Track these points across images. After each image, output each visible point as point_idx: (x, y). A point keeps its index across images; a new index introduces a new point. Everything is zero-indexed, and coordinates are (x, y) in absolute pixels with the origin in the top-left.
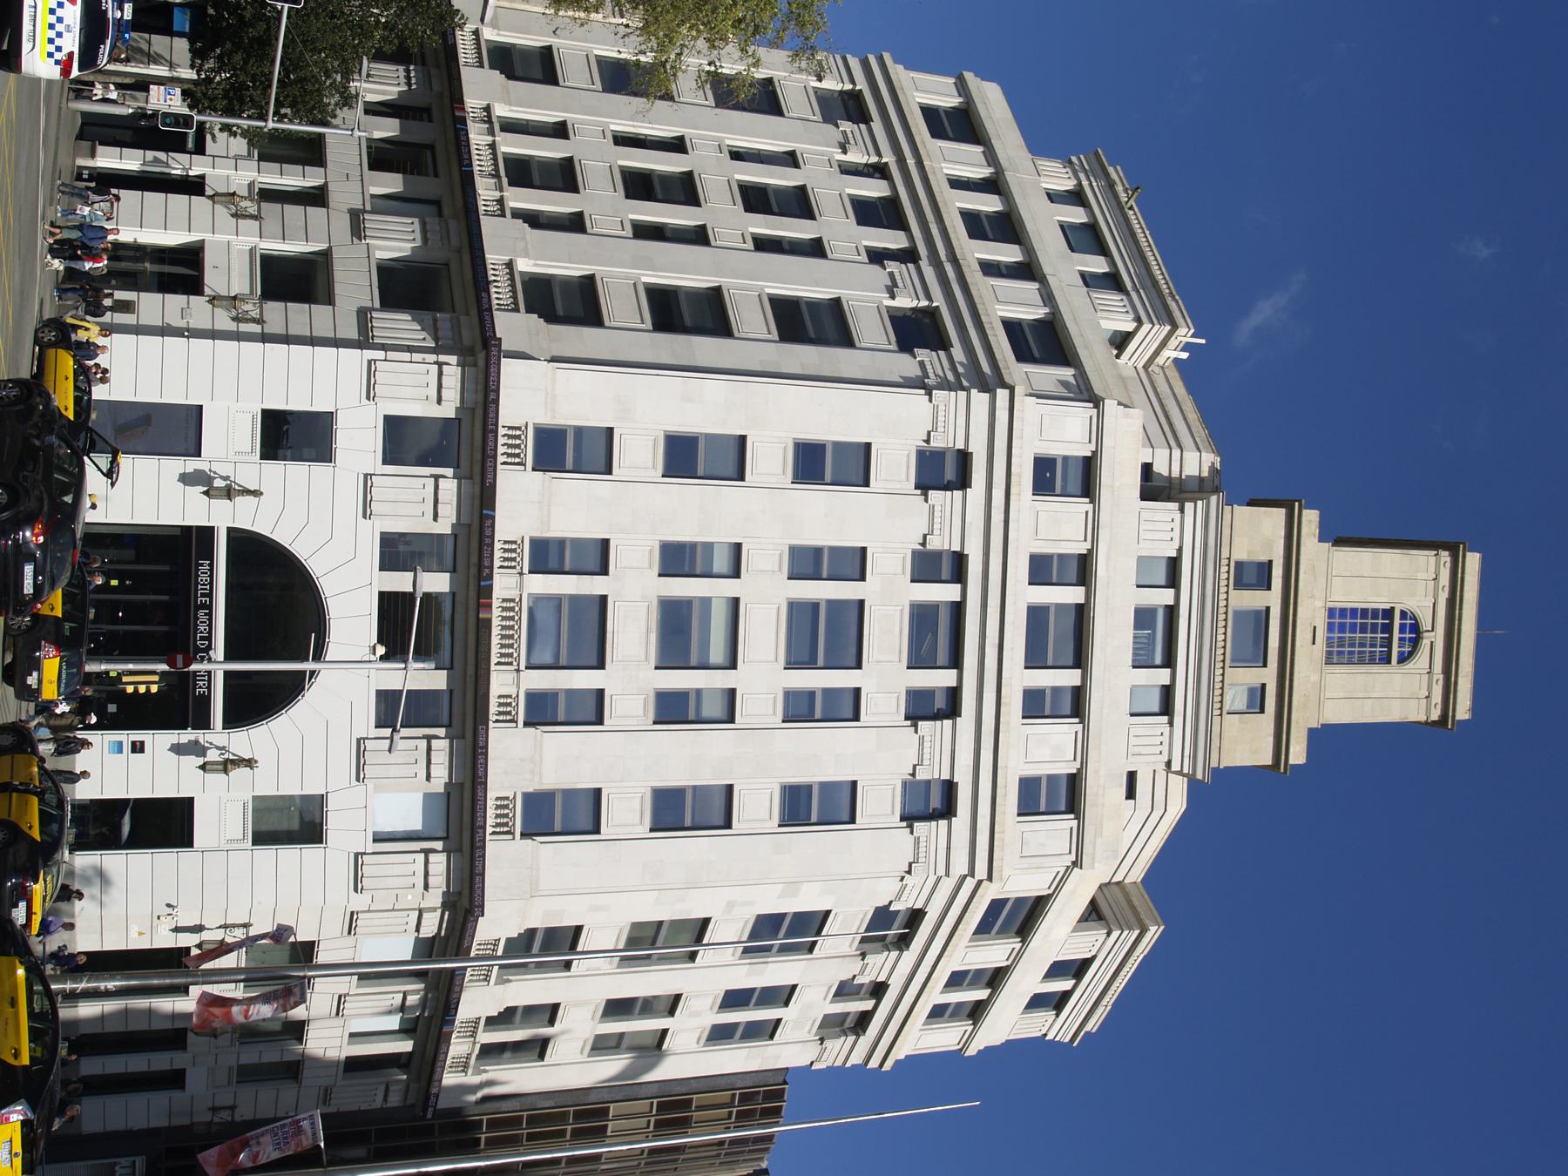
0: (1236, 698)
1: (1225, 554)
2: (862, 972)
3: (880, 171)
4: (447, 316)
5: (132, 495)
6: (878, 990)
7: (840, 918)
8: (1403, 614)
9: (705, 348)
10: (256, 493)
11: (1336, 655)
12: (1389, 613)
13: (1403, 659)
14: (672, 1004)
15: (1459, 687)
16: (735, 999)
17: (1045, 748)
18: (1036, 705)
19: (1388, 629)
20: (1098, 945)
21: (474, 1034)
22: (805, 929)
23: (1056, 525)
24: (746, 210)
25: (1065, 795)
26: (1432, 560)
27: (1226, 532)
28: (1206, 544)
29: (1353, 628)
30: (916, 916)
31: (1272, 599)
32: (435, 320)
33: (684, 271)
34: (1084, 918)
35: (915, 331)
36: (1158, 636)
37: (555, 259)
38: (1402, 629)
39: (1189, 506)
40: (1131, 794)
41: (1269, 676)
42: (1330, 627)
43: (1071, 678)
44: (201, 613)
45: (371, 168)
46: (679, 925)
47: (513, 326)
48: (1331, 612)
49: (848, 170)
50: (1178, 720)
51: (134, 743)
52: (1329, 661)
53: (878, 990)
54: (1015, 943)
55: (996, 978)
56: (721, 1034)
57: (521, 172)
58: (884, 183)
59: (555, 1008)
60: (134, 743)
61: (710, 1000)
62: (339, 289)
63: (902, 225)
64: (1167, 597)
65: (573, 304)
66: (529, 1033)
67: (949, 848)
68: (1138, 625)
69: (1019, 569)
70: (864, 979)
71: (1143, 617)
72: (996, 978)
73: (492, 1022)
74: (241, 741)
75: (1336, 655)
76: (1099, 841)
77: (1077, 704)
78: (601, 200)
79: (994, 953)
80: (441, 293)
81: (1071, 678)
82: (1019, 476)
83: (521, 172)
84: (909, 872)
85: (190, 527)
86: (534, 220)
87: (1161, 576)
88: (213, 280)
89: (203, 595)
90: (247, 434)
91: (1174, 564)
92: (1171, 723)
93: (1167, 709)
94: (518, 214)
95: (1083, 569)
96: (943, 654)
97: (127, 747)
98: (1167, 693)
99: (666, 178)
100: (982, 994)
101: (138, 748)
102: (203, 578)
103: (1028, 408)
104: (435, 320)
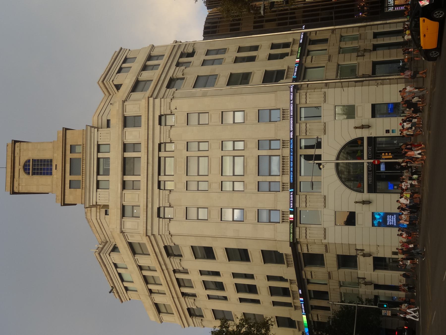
0: (79, 149)
1: (83, 190)
2: (183, 70)
3: (184, 294)
4: (305, 252)
5: (388, 202)
6: (178, 65)
7: (190, 86)
8: (29, 173)
9: (233, 245)
10: (356, 202)
11: (49, 162)
12: (34, 174)
13: (29, 161)
14: (204, 63)
15: (11, 152)
16: (252, 59)
17: (133, 135)
18: (135, 147)
19: (34, 169)
20: (116, 77)
21: (292, 51)
22: (199, 82)
23: (131, 198)
24: (222, 283)
25: (126, 122)
26: (20, 189)
27: (83, 197)
28: (89, 193)
29: (44, 169)
30: (168, 87)
31: (68, 178)
32: (308, 251)
33: (240, 267)
34: (121, 85)
35: (171, 252)
36: (102, 167)
37: (276, 269)
38: (29, 169)
39: (95, 204)
40: (108, 121)
41: (69, 155)
42: (51, 169)
43: (127, 155)
44: (371, 169)
45: (328, 292)
46: (235, 83)
47: (287, 250)
48: (51, 174)
49: (194, 295)
50: (96, 143)
51: (389, 133)
52: (51, 161)
53: (178, 65)
54: (140, 78)
55: (145, 68)
56: (256, 48)
57: (285, 292)
58: (150, 288)
59: (235, 62)
60: (389, 133)
61: (226, 61)
62: (335, 259)
63: (177, 280)
64: (100, 178)
65: (271, 257)
66: (278, 52)
67: (161, 106)
68: (109, 170)
69: (143, 185)
70: (183, 68)
71: (107, 172)
72: (145, 68)
73: (287, 54)
74: (359, 133)
75: (49, 162)
76: (118, 108)
77: (125, 147)
78: (263, 285)
79: (145, 75)
80: (304, 260)
81: (127, 155)
82: (144, 211)
83: (285, 292)
84: (171, 99)
85: (375, 193)
86: (281, 279)
87: (101, 184)
88: (370, 260)
89: (370, 174)
90: (359, 219)
91: (98, 188)
92: (98, 142)
93: (99, 146)
94: (286, 280)
95: (124, 185)
96: (101, 161)
97: (391, 131)
98: (98, 151)
99: (245, 291)
100: (149, 63)
101: (387, 131)
102: (370, 179)
103: (142, 229)
104: (308, 251)
